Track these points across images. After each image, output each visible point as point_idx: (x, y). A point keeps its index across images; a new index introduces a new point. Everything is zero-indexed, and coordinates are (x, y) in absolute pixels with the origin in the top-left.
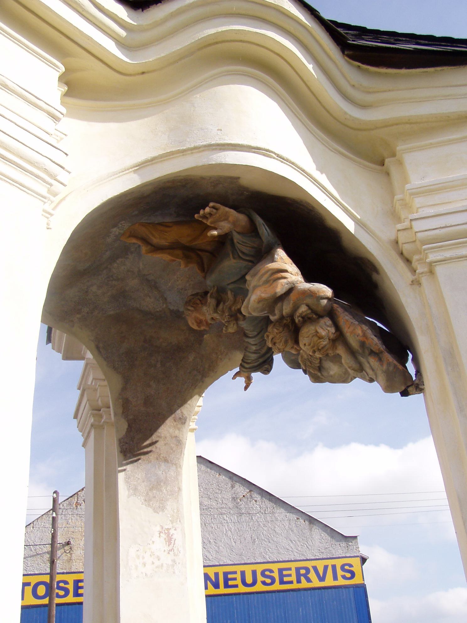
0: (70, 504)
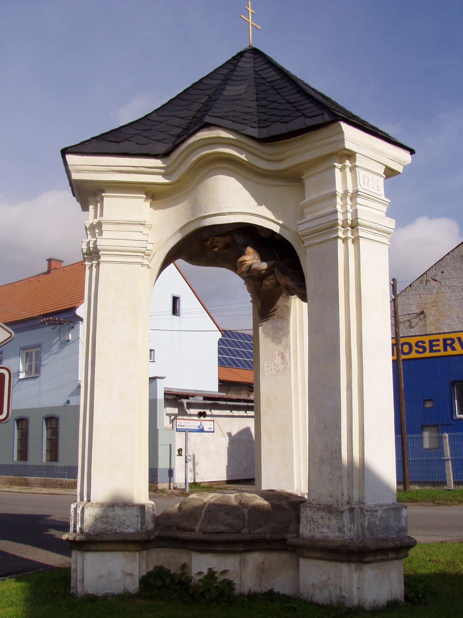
0: (421, 282)
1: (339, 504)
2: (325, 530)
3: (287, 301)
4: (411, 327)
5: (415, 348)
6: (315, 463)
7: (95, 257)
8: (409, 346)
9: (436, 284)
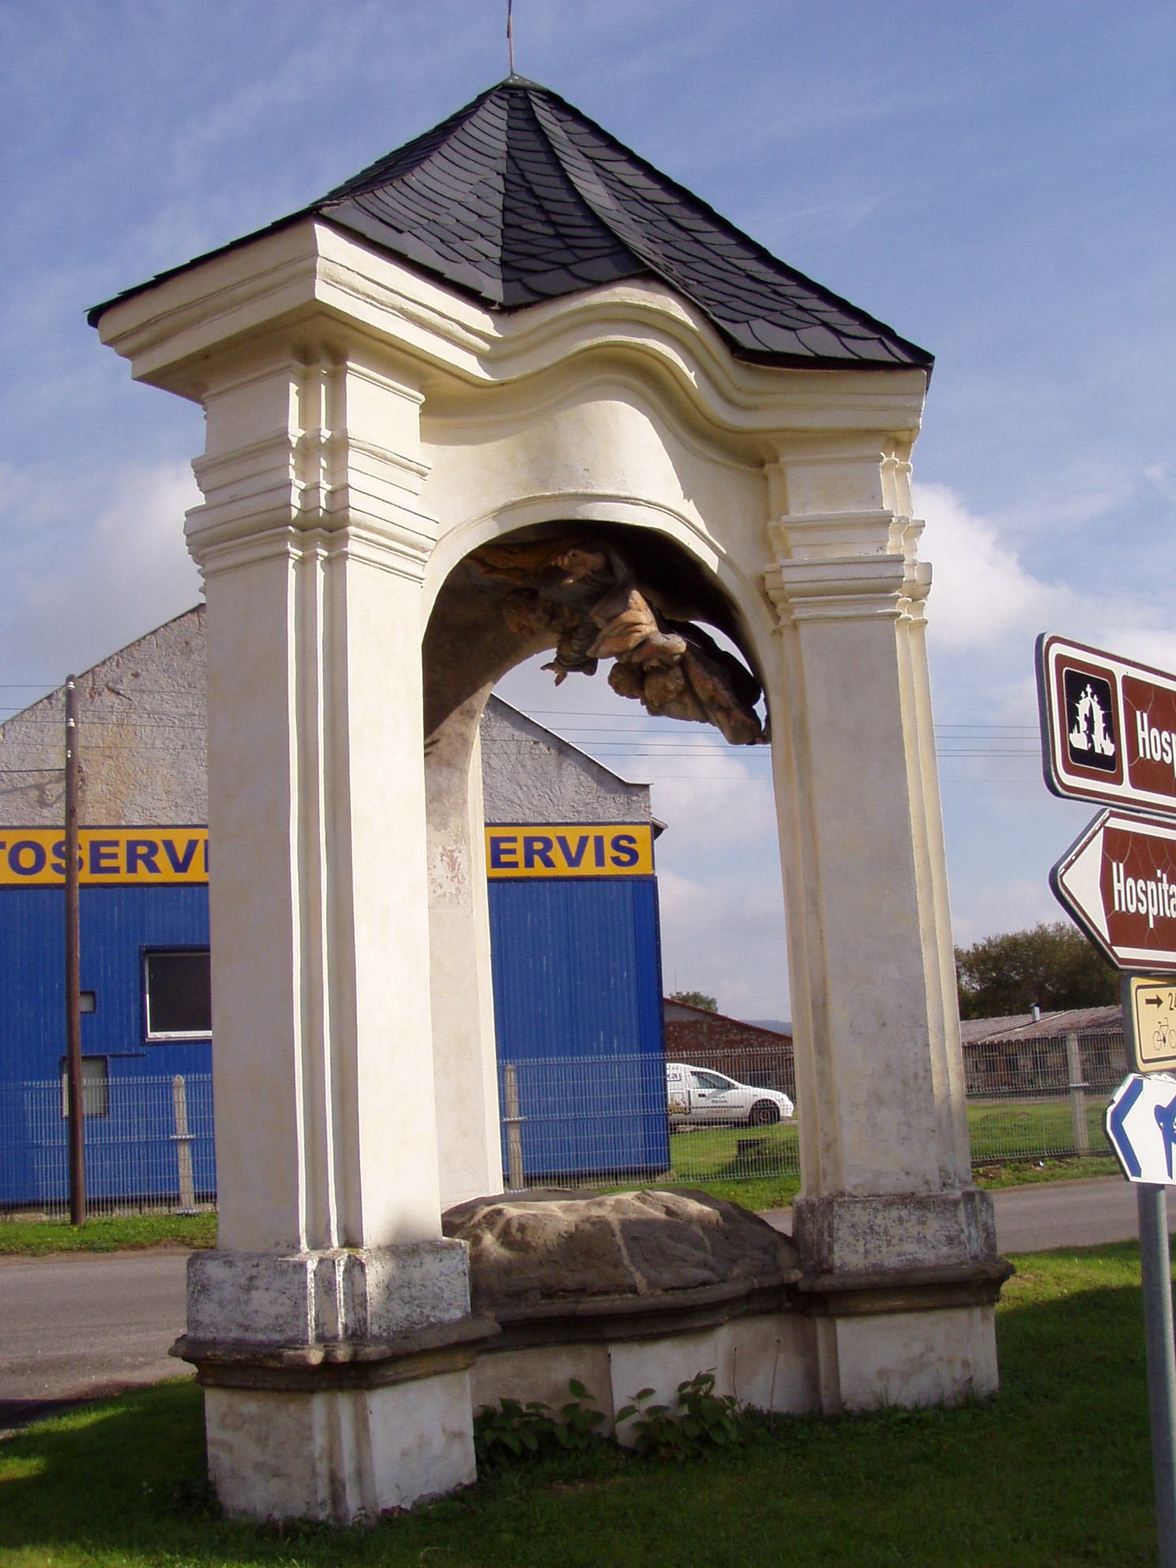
1: (932, 1187)
2: (910, 1247)
3: (466, 725)
4: (42, 803)
5: (51, 859)
6: (856, 1105)
7: (324, 537)
8: (33, 849)
9: (118, 701)
